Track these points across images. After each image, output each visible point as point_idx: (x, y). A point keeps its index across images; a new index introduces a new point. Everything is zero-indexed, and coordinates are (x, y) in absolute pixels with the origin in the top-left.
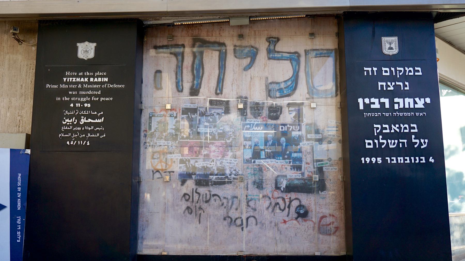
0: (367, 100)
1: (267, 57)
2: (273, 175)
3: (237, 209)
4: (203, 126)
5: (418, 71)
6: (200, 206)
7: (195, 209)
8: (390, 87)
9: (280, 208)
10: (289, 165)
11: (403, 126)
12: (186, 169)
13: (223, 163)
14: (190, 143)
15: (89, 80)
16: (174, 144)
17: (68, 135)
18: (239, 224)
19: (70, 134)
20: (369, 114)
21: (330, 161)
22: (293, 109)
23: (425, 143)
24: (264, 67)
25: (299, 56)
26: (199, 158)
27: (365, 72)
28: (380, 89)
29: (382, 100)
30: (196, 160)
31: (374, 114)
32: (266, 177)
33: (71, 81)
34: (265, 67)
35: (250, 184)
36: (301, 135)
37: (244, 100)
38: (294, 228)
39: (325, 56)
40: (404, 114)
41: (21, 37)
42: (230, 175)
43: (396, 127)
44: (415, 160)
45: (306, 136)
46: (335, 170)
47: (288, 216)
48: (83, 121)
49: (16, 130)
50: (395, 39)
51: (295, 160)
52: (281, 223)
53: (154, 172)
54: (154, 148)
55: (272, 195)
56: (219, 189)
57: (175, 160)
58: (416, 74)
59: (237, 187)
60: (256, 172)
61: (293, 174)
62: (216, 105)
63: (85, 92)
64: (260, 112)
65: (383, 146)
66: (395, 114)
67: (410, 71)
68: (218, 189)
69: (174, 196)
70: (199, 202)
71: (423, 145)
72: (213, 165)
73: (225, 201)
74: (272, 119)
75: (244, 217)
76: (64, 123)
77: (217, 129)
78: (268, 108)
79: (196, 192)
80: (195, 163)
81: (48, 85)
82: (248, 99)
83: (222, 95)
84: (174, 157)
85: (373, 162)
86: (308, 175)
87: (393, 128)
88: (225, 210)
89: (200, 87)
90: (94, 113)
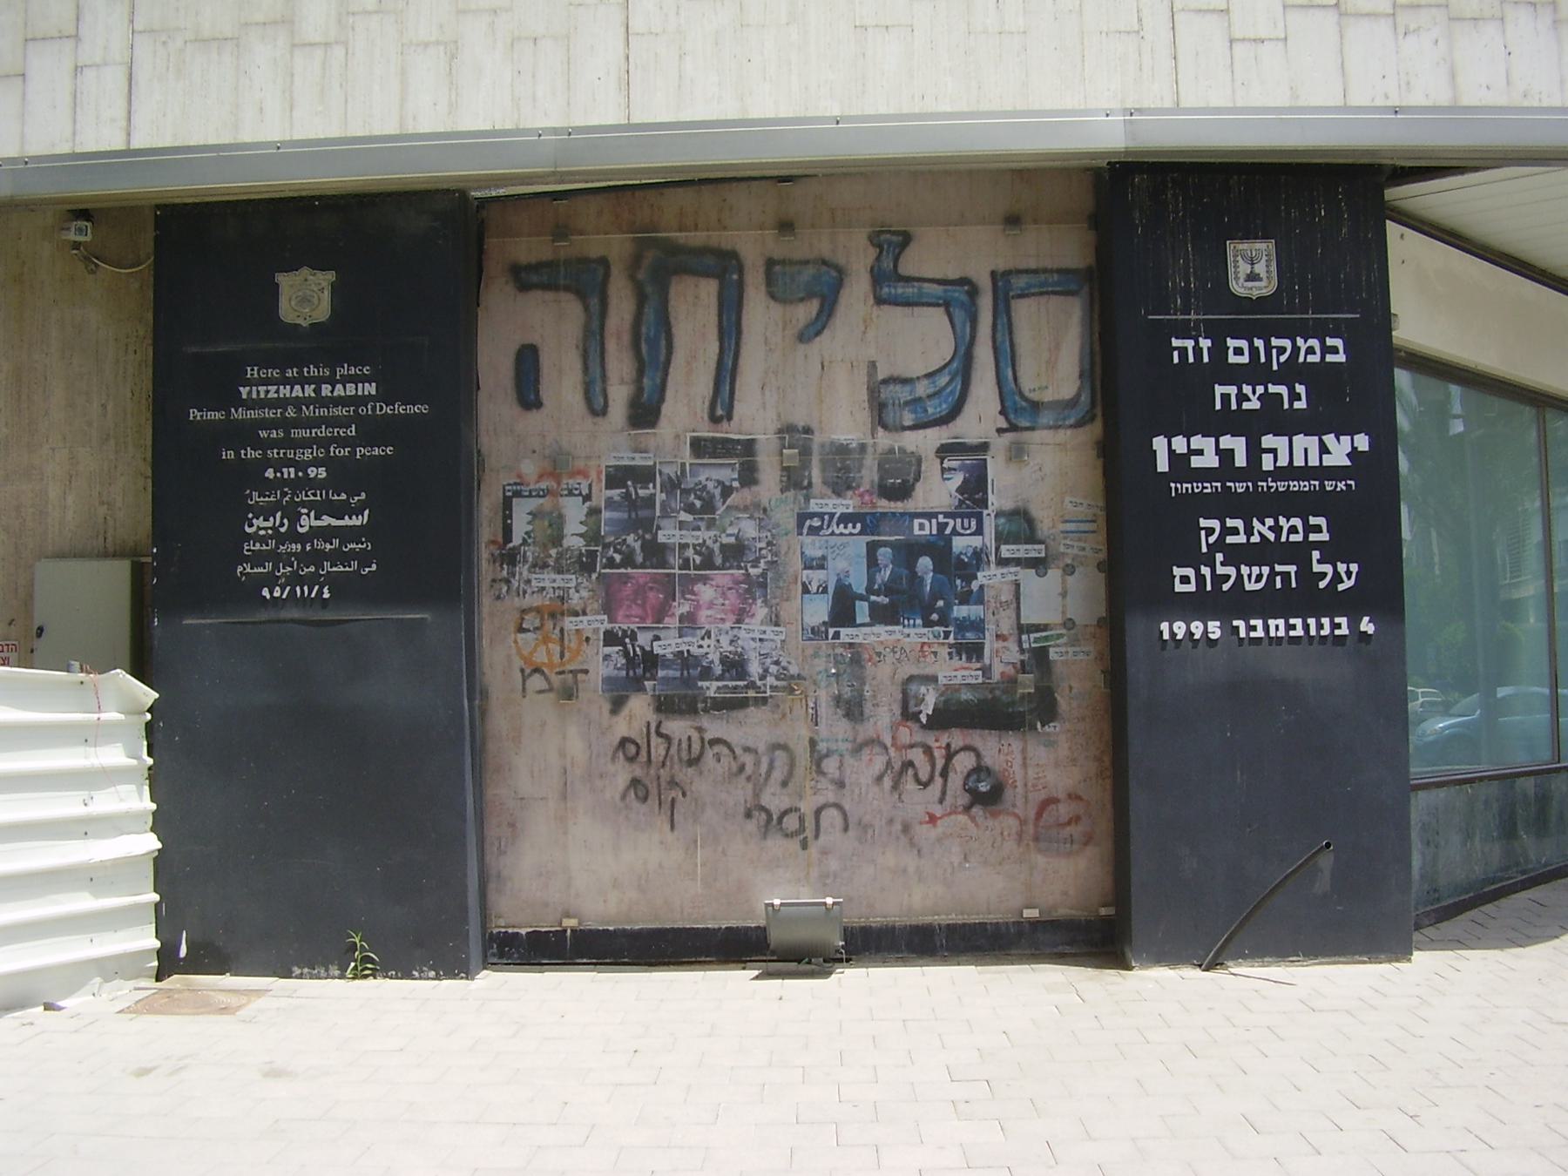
0: (1179, 444)
1: (872, 296)
3: (784, 784)
4: (673, 525)
6: (672, 777)
7: (655, 784)
8: (1249, 400)
9: (916, 775)
10: (943, 644)
12: (624, 661)
14: (634, 578)
15: (317, 391)
16: (586, 583)
20: (1185, 485)
21: (1069, 629)
22: (954, 464)
23: (1349, 574)
24: (863, 329)
25: (973, 291)
27: (1176, 354)
28: (1218, 406)
29: (1227, 442)
31: (1200, 485)
35: (824, 705)
37: (794, 435)
40: (1289, 486)
42: (762, 678)
44: (1320, 626)
45: (997, 549)
46: (1086, 657)
47: (941, 801)
51: (963, 626)
52: (921, 823)
53: (526, 674)
55: (893, 738)
56: (728, 722)
57: (590, 635)
58: (1330, 358)
59: (784, 716)
61: (956, 670)
65: (1226, 587)
66: (1262, 487)
67: (1309, 350)
69: (590, 746)
71: (1342, 582)
72: (709, 646)
73: (748, 759)
74: (890, 500)
75: (807, 807)
76: (248, 530)
78: (876, 462)
79: (659, 734)
82: (812, 433)
83: (732, 422)
84: (585, 623)
85: (1193, 634)
86: (1002, 674)
88: (750, 786)
89: (662, 399)
90: (339, 495)
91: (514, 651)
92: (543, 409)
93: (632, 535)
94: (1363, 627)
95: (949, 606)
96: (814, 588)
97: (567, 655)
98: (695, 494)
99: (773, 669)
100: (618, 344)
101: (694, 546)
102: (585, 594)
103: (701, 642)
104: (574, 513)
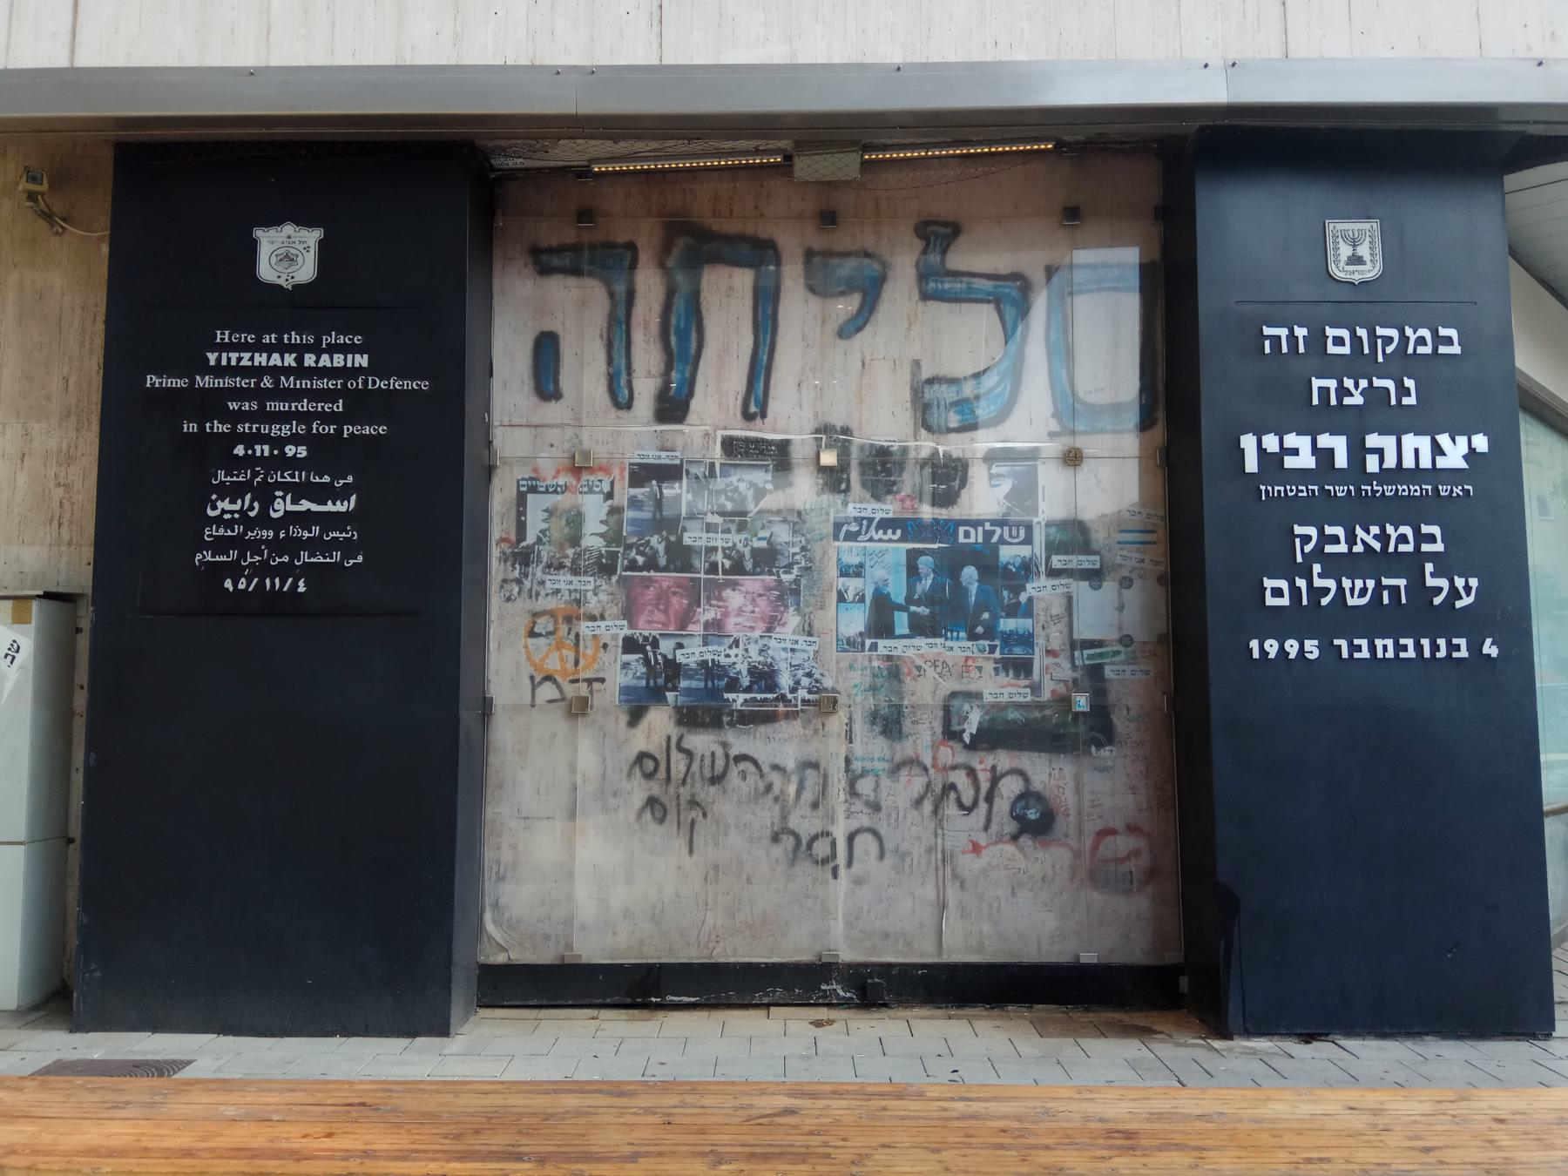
0: (1271, 443)
1: (917, 292)
2: (936, 690)
3: (815, 805)
5: (1449, 341)
6: (693, 795)
7: (674, 803)
8: (1352, 395)
10: (988, 659)
11: (1396, 531)
12: (644, 670)
13: (769, 651)
14: (657, 581)
15: (300, 360)
16: (604, 587)
17: (228, 557)
18: (825, 856)
19: (234, 554)
20: (1276, 488)
21: (1125, 646)
23: (1468, 589)
24: (907, 325)
26: (687, 635)
27: (1267, 343)
28: (1315, 401)
29: (1325, 441)
30: (679, 640)
31: (1294, 488)
32: (914, 698)
33: (233, 363)
34: (910, 324)
36: (1031, 559)
38: (1007, 867)
39: (1116, 289)
40: (1397, 490)
41: (58, 207)
42: (793, 690)
43: (1372, 535)
44: (1435, 648)
45: (1048, 559)
46: (1144, 676)
47: (986, 828)
48: (280, 507)
49: (49, 536)
50: (1370, 227)
51: (1010, 639)
52: (964, 852)
54: (537, 600)
55: (934, 759)
58: (1442, 350)
60: (879, 681)
61: (1002, 687)
62: (747, 455)
63: (287, 404)
64: (892, 479)
65: (1325, 601)
68: (752, 737)
69: (604, 761)
70: (689, 780)
71: (1461, 598)
72: (736, 656)
73: (776, 778)
75: (840, 832)
76: (211, 513)
77: (749, 537)
79: (680, 749)
80: (675, 649)
81: (151, 379)
83: (766, 420)
84: (603, 628)
85: (1288, 654)
86: (1053, 692)
87: (1362, 539)
88: (777, 808)
89: (691, 394)
91: (524, 657)
92: (561, 401)
93: (656, 537)
94: (1486, 650)
95: (995, 619)
96: (850, 596)
97: (582, 661)
98: (726, 495)
99: (805, 681)
100: (645, 335)
101: (724, 549)
102: (603, 597)
103: (728, 651)
104: (594, 510)
